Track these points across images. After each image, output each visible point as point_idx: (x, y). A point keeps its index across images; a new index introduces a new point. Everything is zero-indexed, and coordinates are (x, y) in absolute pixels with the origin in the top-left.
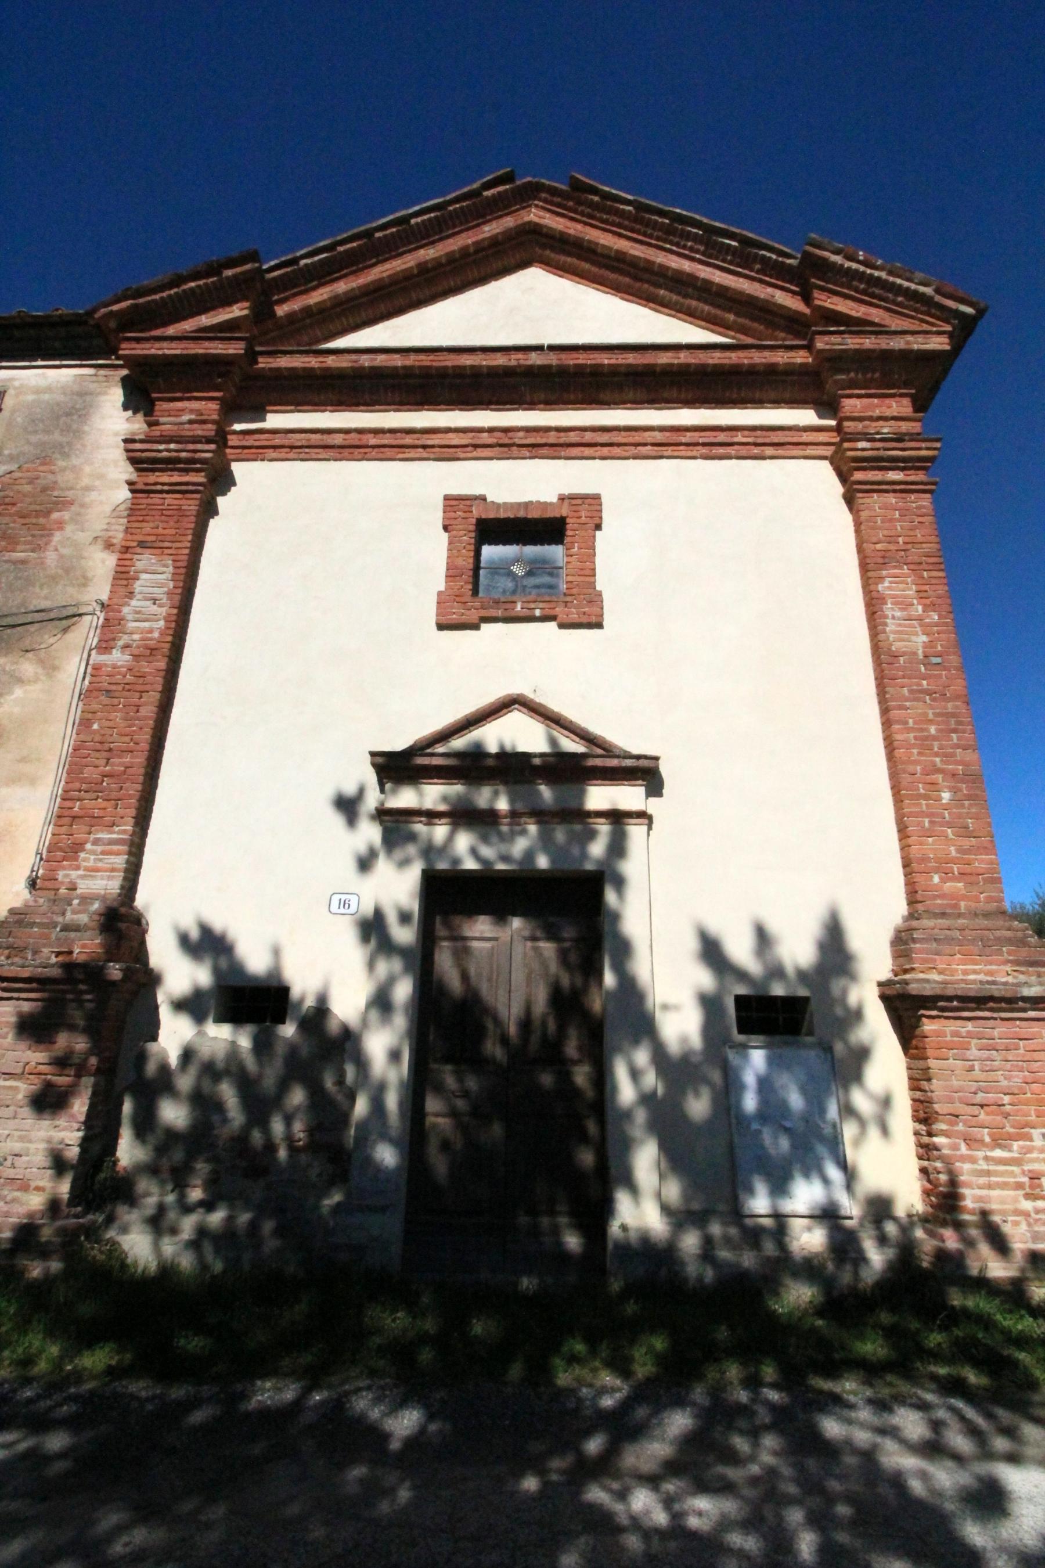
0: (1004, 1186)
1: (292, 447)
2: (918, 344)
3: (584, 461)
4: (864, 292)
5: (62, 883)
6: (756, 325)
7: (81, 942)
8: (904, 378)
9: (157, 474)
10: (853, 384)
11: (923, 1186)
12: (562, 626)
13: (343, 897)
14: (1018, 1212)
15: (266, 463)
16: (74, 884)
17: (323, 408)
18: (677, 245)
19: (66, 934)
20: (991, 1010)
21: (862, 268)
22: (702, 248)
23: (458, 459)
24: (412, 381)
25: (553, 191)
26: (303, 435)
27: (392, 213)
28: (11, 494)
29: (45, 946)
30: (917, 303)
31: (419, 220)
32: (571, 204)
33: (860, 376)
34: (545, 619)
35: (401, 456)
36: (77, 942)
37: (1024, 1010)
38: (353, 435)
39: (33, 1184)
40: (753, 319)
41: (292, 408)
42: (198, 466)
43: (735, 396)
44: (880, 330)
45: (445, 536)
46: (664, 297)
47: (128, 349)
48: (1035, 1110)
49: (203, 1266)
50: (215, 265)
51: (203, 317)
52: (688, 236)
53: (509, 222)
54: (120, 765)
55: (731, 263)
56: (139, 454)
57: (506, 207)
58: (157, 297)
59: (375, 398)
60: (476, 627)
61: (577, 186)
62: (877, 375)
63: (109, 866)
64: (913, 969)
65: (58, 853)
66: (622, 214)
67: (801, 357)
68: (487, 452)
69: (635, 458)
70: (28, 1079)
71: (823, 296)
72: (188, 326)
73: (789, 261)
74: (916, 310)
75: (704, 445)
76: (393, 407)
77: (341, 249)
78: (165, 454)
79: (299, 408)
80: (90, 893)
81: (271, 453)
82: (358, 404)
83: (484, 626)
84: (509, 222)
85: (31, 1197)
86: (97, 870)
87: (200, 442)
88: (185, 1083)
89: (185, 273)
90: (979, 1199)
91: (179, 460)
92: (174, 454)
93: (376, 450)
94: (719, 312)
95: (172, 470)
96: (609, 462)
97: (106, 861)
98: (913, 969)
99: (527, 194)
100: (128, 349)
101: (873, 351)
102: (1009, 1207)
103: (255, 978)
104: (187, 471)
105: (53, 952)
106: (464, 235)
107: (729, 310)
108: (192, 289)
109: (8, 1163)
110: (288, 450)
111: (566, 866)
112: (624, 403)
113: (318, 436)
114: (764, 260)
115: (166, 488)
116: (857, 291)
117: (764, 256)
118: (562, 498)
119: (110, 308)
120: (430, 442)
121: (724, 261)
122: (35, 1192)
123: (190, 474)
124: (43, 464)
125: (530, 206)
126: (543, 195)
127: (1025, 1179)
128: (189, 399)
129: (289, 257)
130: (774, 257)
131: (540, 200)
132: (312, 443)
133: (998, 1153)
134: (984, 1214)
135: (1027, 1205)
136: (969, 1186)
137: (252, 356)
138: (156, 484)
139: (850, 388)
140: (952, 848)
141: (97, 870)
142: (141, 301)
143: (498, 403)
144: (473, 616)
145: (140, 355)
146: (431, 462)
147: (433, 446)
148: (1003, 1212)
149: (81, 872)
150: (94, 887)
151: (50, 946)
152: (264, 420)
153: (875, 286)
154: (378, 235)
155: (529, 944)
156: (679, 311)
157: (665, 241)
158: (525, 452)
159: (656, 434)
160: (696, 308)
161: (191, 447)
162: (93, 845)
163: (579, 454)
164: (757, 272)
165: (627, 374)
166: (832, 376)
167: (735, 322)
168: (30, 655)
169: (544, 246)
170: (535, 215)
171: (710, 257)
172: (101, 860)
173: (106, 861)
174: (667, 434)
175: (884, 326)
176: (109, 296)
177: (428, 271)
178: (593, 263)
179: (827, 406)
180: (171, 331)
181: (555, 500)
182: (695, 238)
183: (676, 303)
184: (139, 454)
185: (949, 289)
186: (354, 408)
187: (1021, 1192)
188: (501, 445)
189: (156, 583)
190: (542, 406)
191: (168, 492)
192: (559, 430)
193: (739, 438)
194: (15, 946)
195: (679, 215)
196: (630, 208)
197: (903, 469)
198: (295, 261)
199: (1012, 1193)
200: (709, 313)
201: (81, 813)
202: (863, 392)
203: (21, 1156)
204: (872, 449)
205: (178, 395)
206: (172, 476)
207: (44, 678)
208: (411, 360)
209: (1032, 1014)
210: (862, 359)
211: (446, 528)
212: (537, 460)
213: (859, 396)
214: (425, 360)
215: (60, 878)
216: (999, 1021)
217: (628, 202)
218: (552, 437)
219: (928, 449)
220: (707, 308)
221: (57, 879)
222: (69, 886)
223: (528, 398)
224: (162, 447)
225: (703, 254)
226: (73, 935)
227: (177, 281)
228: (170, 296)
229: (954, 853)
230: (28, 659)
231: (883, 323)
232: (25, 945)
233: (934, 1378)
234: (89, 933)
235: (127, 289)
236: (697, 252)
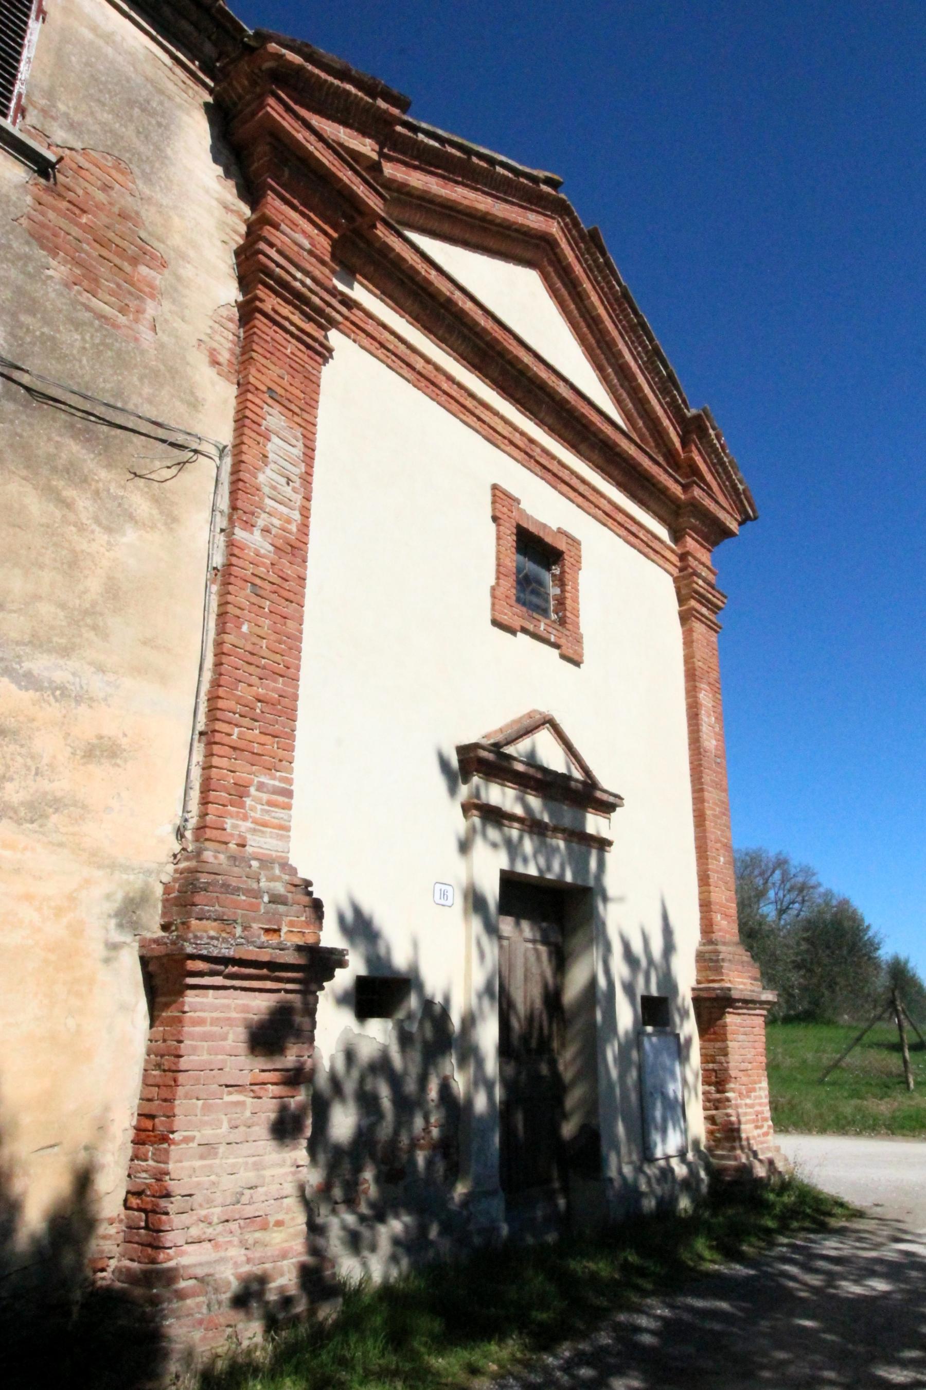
1: (382, 345)
2: (722, 515)
4: (714, 465)
5: (232, 835)
6: (650, 440)
7: (289, 918)
9: (279, 300)
11: (707, 1128)
12: (563, 657)
13: (444, 887)
15: (356, 346)
16: (244, 838)
17: (403, 313)
18: (633, 342)
19: (274, 906)
21: (718, 446)
24: (478, 342)
25: (576, 224)
26: (392, 337)
27: (491, 149)
28: (80, 192)
29: (254, 920)
32: (582, 245)
34: (556, 646)
35: (464, 418)
36: (284, 918)
37: (755, 1009)
38: (430, 367)
39: (272, 1220)
40: (652, 436)
41: (378, 292)
42: (323, 321)
45: (493, 526)
46: (609, 375)
50: (379, 89)
51: (342, 129)
52: (642, 343)
54: (274, 690)
55: (656, 383)
56: (272, 265)
57: (544, 208)
58: (323, 75)
59: (447, 336)
60: (513, 632)
63: (276, 821)
64: (722, 980)
65: (223, 794)
66: (611, 288)
67: (677, 490)
68: (516, 453)
70: (252, 1091)
71: (278, 203)
73: (685, 411)
74: (731, 496)
75: (626, 529)
76: (455, 354)
78: (297, 285)
79: (383, 297)
80: (263, 854)
81: (366, 342)
85: (274, 1235)
86: (265, 825)
87: (334, 296)
88: (350, 1087)
89: (353, 72)
91: (307, 302)
92: (304, 290)
93: (445, 396)
94: (635, 414)
95: (296, 307)
96: (580, 510)
97: (273, 814)
98: (722, 980)
99: (558, 208)
103: (397, 972)
104: (310, 319)
105: (262, 929)
106: (516, 209)
107: (641, 417)
108: (348, 93)
109: (245, 1199)
110: (378, 345)
114: (673, 398)
115: (292, 329)
116: (711, 460)
117: (675, 396)
118: (560, 531)
119: (284, 51)
121: (653, 378)
122: (275, 1228)
123: (311, 324)
124: (117, 168)
125: (554, 218)
126: (568, 220)
128: (303, 214)
129: (415, 122)
130: (680, 401)
131: (563, 220)
132: (399, 352)
138: (287, 319)
141: (265, 825)
142: (310, 67)
143: (522, 405)
144: (517, 623)
145: (283, 127)
146: (480, 437)
147: (484, 422)
149: (249, 824)
150: (265, 846)
151: (259, 921)
152: (351, 287)
155: (530, 945)
156: (613, 393)
157: (627, 332)
158: (538, 469)
159: (605, 502)
160: (624, 400)
161: (328, 298)
162: (257, 790)
163: (565, 492)
164: (667, 403)
165: (601, 441)
166: (689, 517)
167: (640, 428)
168: (141, 482)
169: (551, 263)
171: (647, 368)
172: (267, 812)
173: (273, 814)
176: (287, 37)
178: (578, 309)
179: (677, 535)
180: (316, 121)
181: (555, 528)
182: (645, 347)
183: (615, 386)
184: (272, 265)
186: (426, 332)
188: (526, 453)
189: (289, 457)
190: (546, 428)
191: (292, 335)
192: (560, 463)
193: (641, 534)
194: (225, 918)
195: (645, 323)
196: (618, 288)
197: (708, 609)
200: (629, 410)
201: (241, 744)
203: (256, 1187)
205: (295, 202)
206: (293, 313)
207: (163, 528)
208: (488, 324)
211: (495, 519)
212: (543, 482)
214: (499, 334)
215: (228, 826)
217: (620, 284)
218: (554, 467)
220: (630, 405)
221: (225, 829)
222: (239, 842)
223: (542, 415)
224: (299, 275)
225: (644, 363)
226: (281, 908)
227: (343, 75)
228: (332, 84)
230: (138, 488)
232: (232, 918)
234: (296, 907)
235: (307, 45)
236: (641, 358)
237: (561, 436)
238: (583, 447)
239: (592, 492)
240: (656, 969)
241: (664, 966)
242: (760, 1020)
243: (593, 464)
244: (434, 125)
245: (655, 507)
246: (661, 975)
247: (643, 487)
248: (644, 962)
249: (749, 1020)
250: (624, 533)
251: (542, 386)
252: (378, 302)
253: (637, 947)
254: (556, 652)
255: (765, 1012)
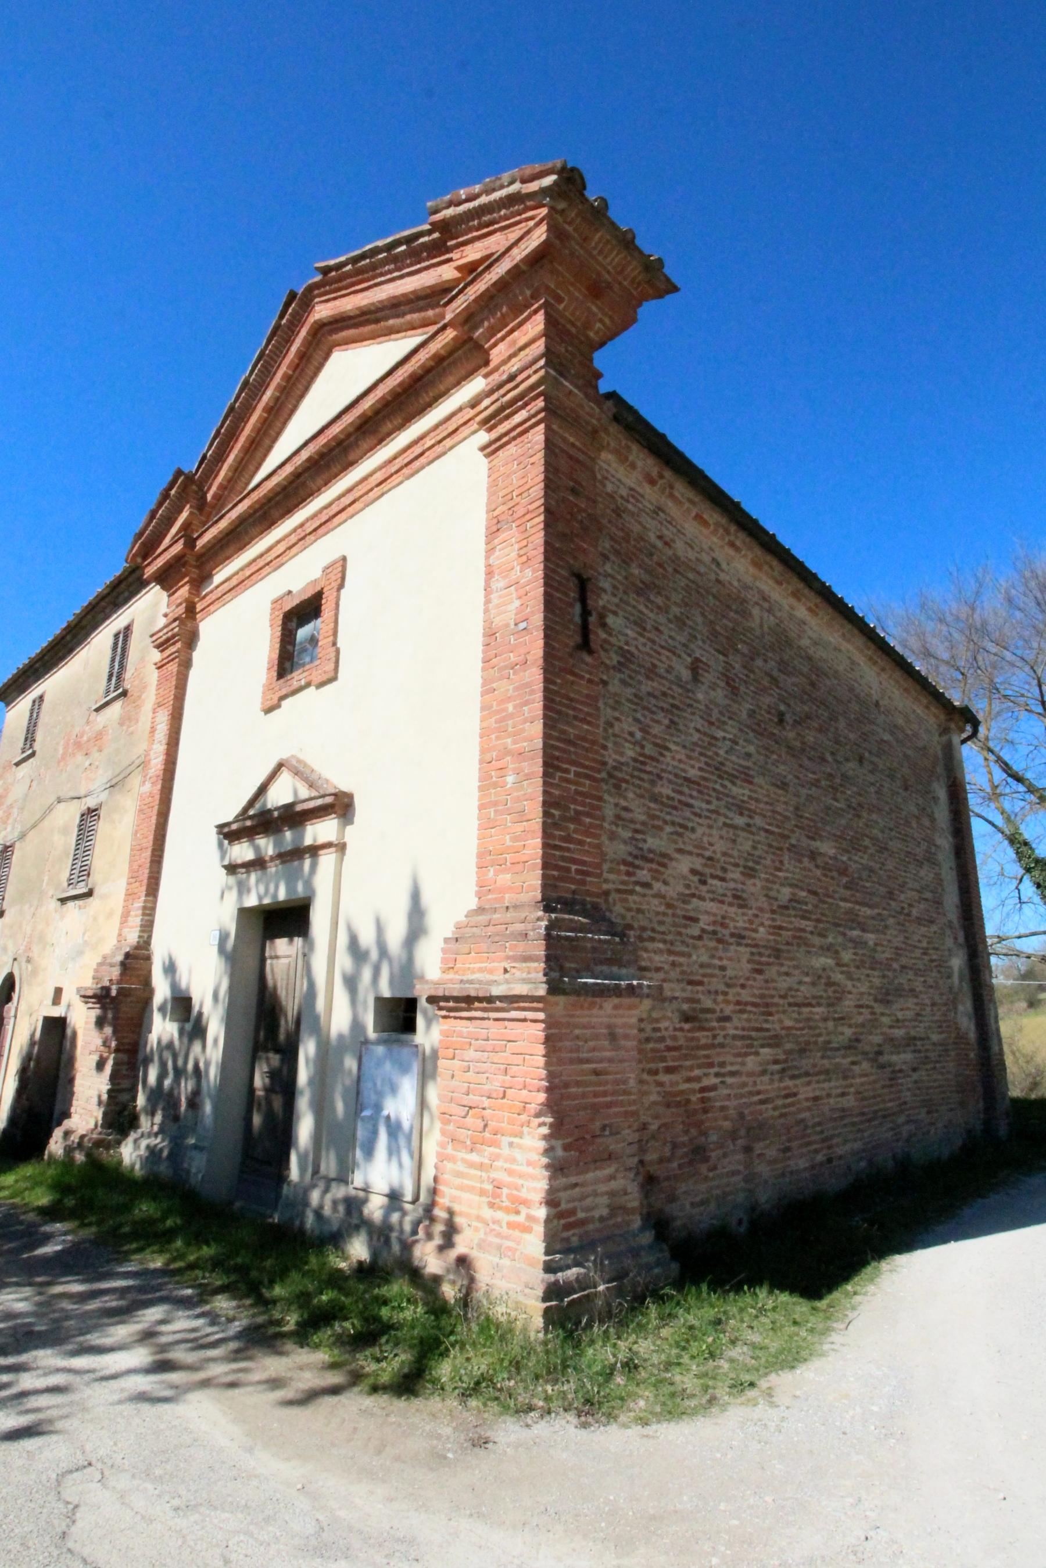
0: (470, 1189)
3: (342, 526)
8: (528, 293)
10: (492, 331)
12: (321, 685)
14: (479, 1218)
20: (484, 1010)
22: (392, 266)
23: (283, 564)
30: (500, 210)
31: (253, 376)
33: (492, 320)
34: (308, 685)
43: (427, 400)
44: (489, 261)
47: (149, 571)
48: (509, 1117)
49: (133, 1166)
53: (303, 332)
61: (326, 271)
62: (504, 309)
69: (368, 505)
72: (167, 541)
77: (223, 431)
82: (245, 546)
83: (284, 703)
84: (303, 332)
86: (755, 812)
90: (453, 1199)
99: (306, 301)
100: (149, 571)
101: (487, 290)
102: (474, 1212)
111: (293, 897)
112: (365, 454)
113: (226, 584)
120: (269, 559)
125: (314, 307)
127: (489, 1187)
133: (474, 1157)
134: (451, 1213)
135: (487, 1213)
136: (447, 1184)
137: (190, 543)
139: (494, 335)
140: (508, 837)
148: (467, 1216)
153: (484, 214)
154: (237, 405)
170: (322, 311)
174: (384, 470)
175: (492, 254)
177: (272, 408)
185: (528, 171)
187: (485, 1199)
191: (168, 662)
198: (204, 457)
199: (477, 1198)
202: (503, 333)
204: (492, 403)
209: (514, 1014)
210: (487, 301)
213: (503, 339)
216: (491, 1021)
219: (536, 372)
229: (508, 843)
231: (488, 252)
233: (136, 1260)
237: (336, 476)
238: (351, 457)
239: (364, 484)
240: (390, 961)
241: (404, 957)
242: (537, 1031)
243: (341, 472)
244: (414, 226)
245: (451, 379)
246: (396, 970)
247: (432, 383)
248: (374, 955)
249: (518, 1029)
250: (267, 569)
251: (297, 475)
252: (316, 500)
253: (367, 938)
254: (312, 688)
255: (541, 1016)
